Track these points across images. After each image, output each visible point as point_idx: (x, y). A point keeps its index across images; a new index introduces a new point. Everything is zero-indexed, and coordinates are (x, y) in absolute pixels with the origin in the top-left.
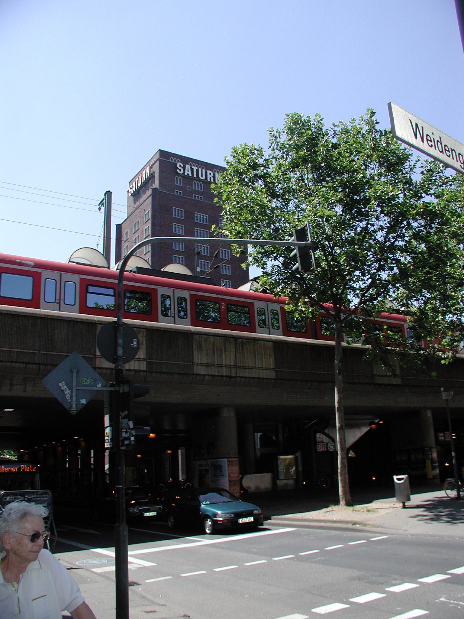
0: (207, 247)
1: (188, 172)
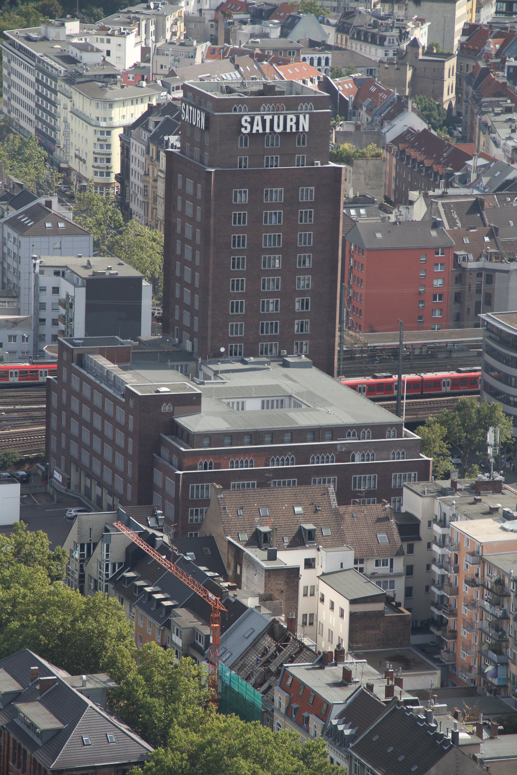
0: (311, 191)
1: (258, 128)
